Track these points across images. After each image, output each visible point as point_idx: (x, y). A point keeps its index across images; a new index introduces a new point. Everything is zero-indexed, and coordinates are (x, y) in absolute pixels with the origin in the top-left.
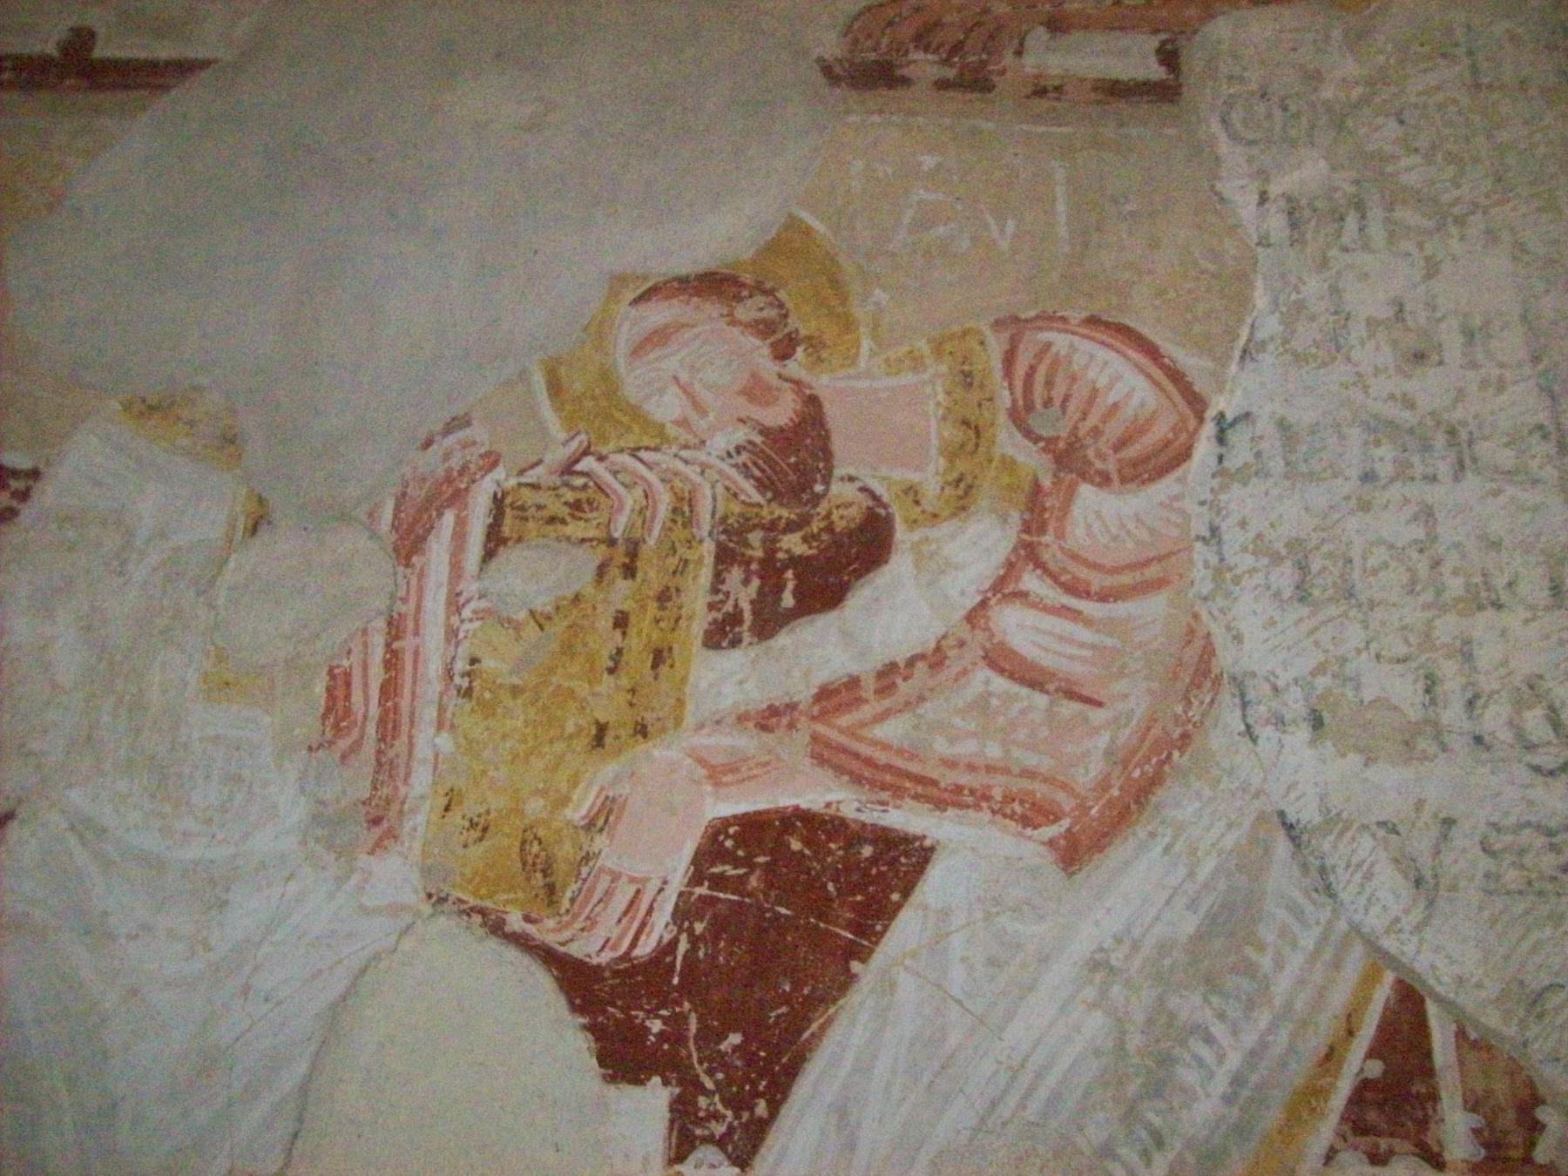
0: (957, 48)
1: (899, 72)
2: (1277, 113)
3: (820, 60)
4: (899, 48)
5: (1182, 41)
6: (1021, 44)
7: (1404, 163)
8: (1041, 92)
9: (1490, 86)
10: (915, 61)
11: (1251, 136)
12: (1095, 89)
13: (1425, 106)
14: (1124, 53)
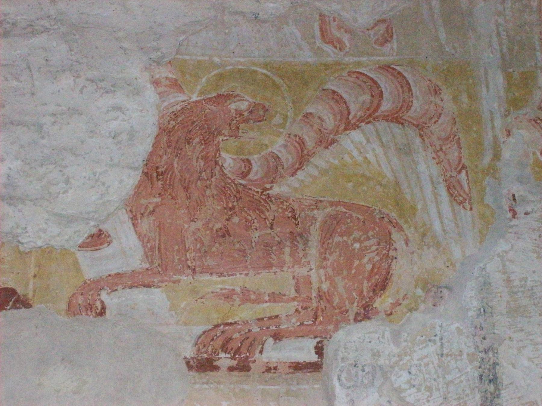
0: (238, 351)
1: (215, 364)
2: (360, 373)
3: (185, 358)
4: (215, 352)
5: (325, 342)
6: (262, 348)
7: (409, 392)
8: (269, 370)
9: (447, 355)
10: (221, 358)
11: (349, 384)
12: (290, 367)
13: (420, 365)
14: (301, 349)
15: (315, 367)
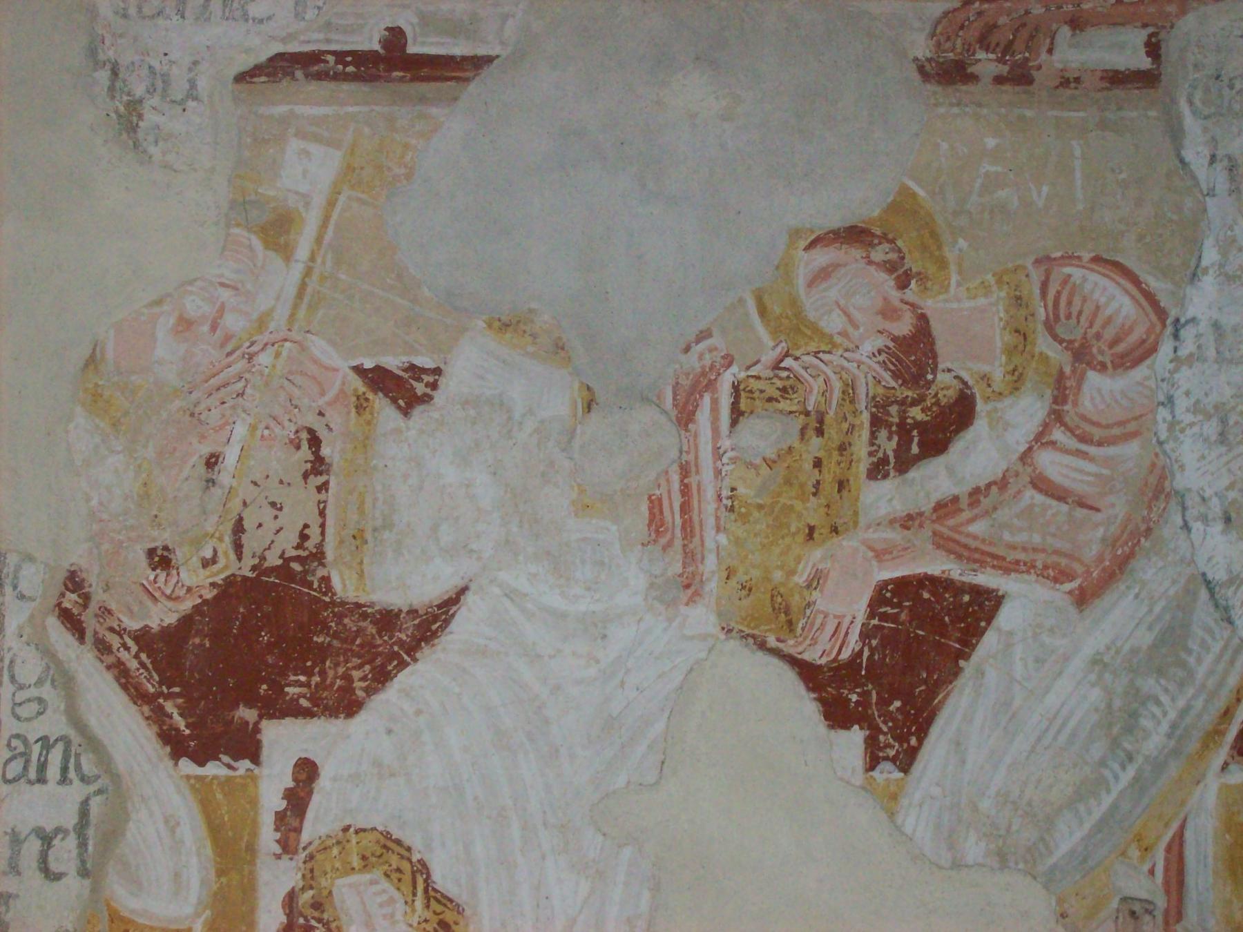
15: (1147, 79)
